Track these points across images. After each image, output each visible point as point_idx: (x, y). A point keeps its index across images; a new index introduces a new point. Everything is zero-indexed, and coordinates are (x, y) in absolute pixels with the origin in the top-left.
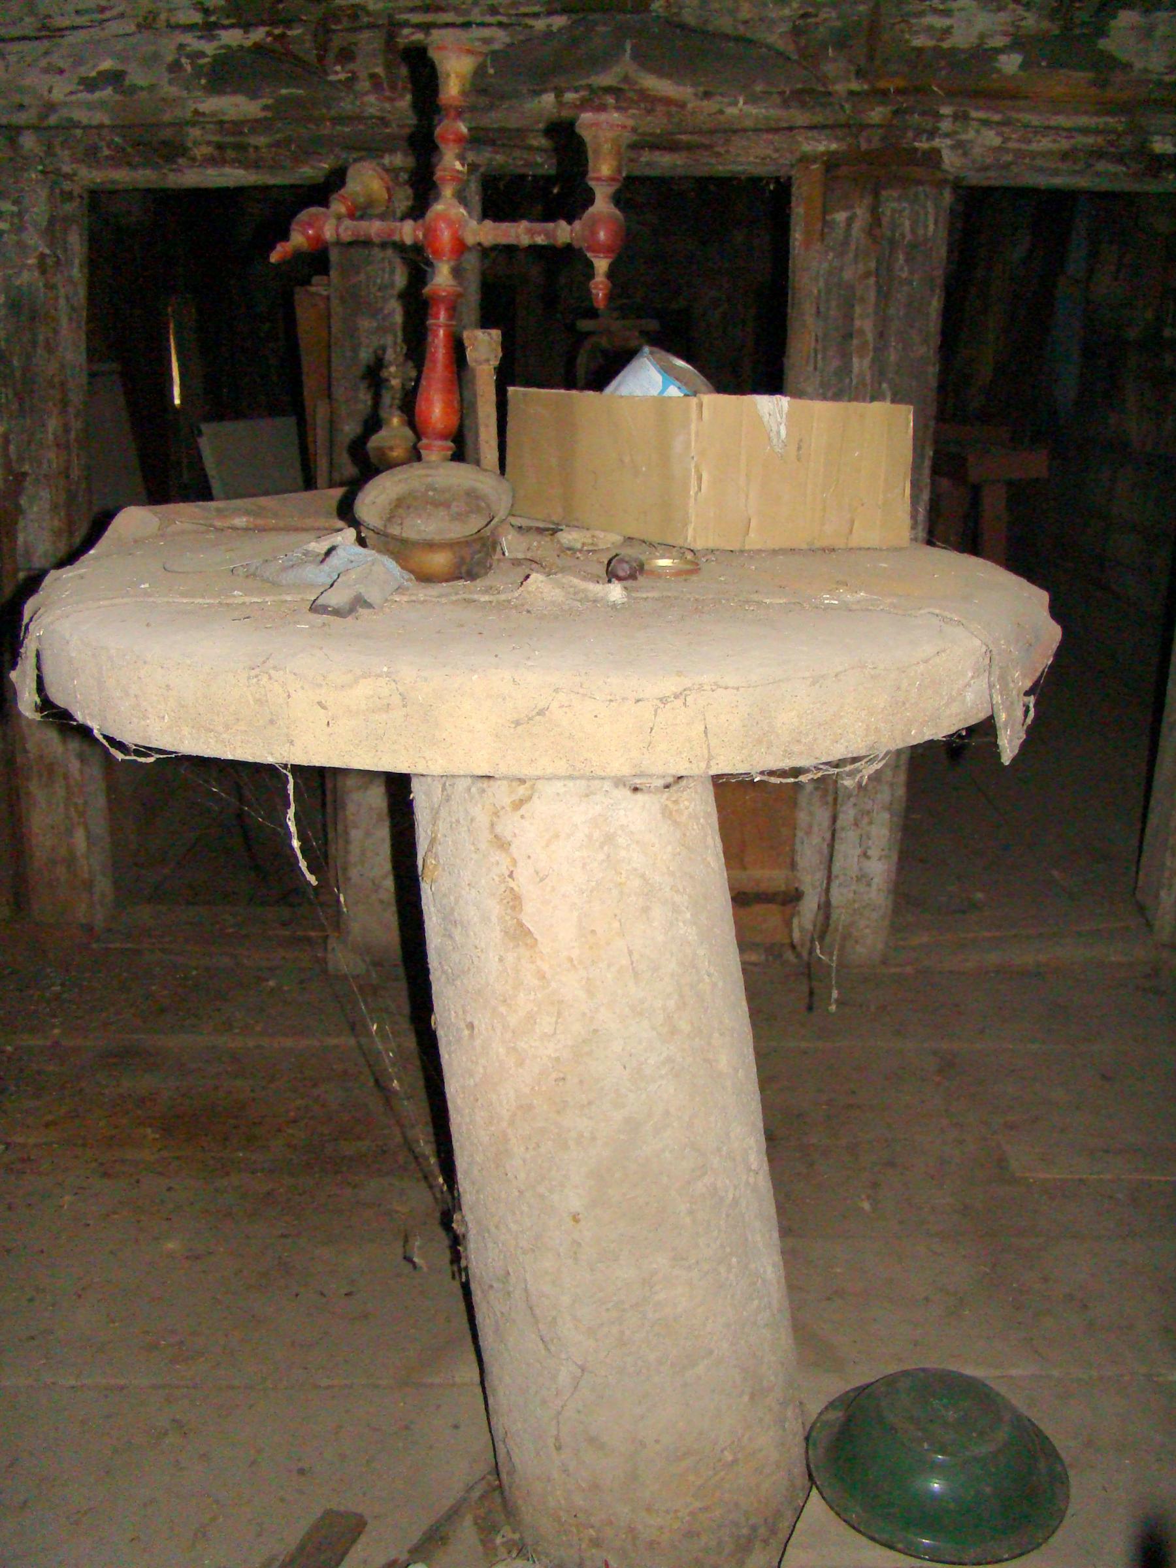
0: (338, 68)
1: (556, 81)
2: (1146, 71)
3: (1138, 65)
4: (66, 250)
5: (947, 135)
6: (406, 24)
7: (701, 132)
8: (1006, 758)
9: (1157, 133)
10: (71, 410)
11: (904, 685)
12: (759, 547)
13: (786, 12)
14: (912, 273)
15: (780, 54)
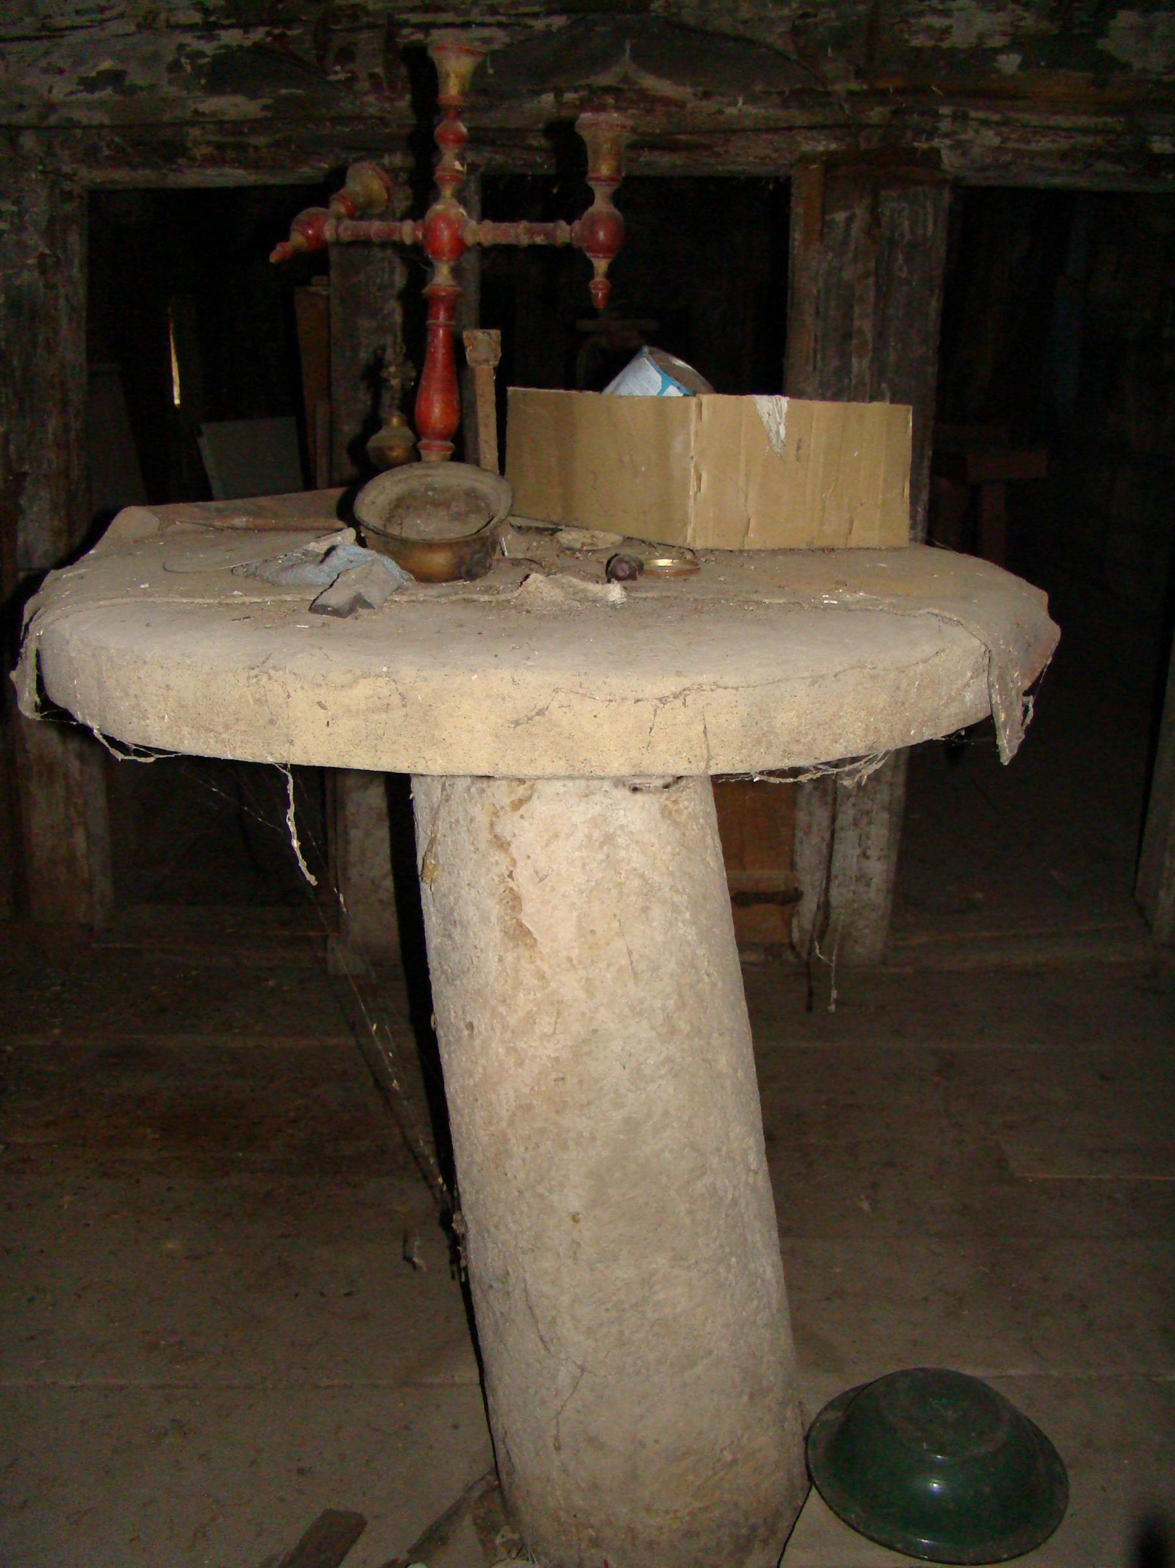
0: (338, 68)
4: (65, 250)
6: (406, 24)
8: (1006, 758)
12: (758, 547)
13: (786, 12)
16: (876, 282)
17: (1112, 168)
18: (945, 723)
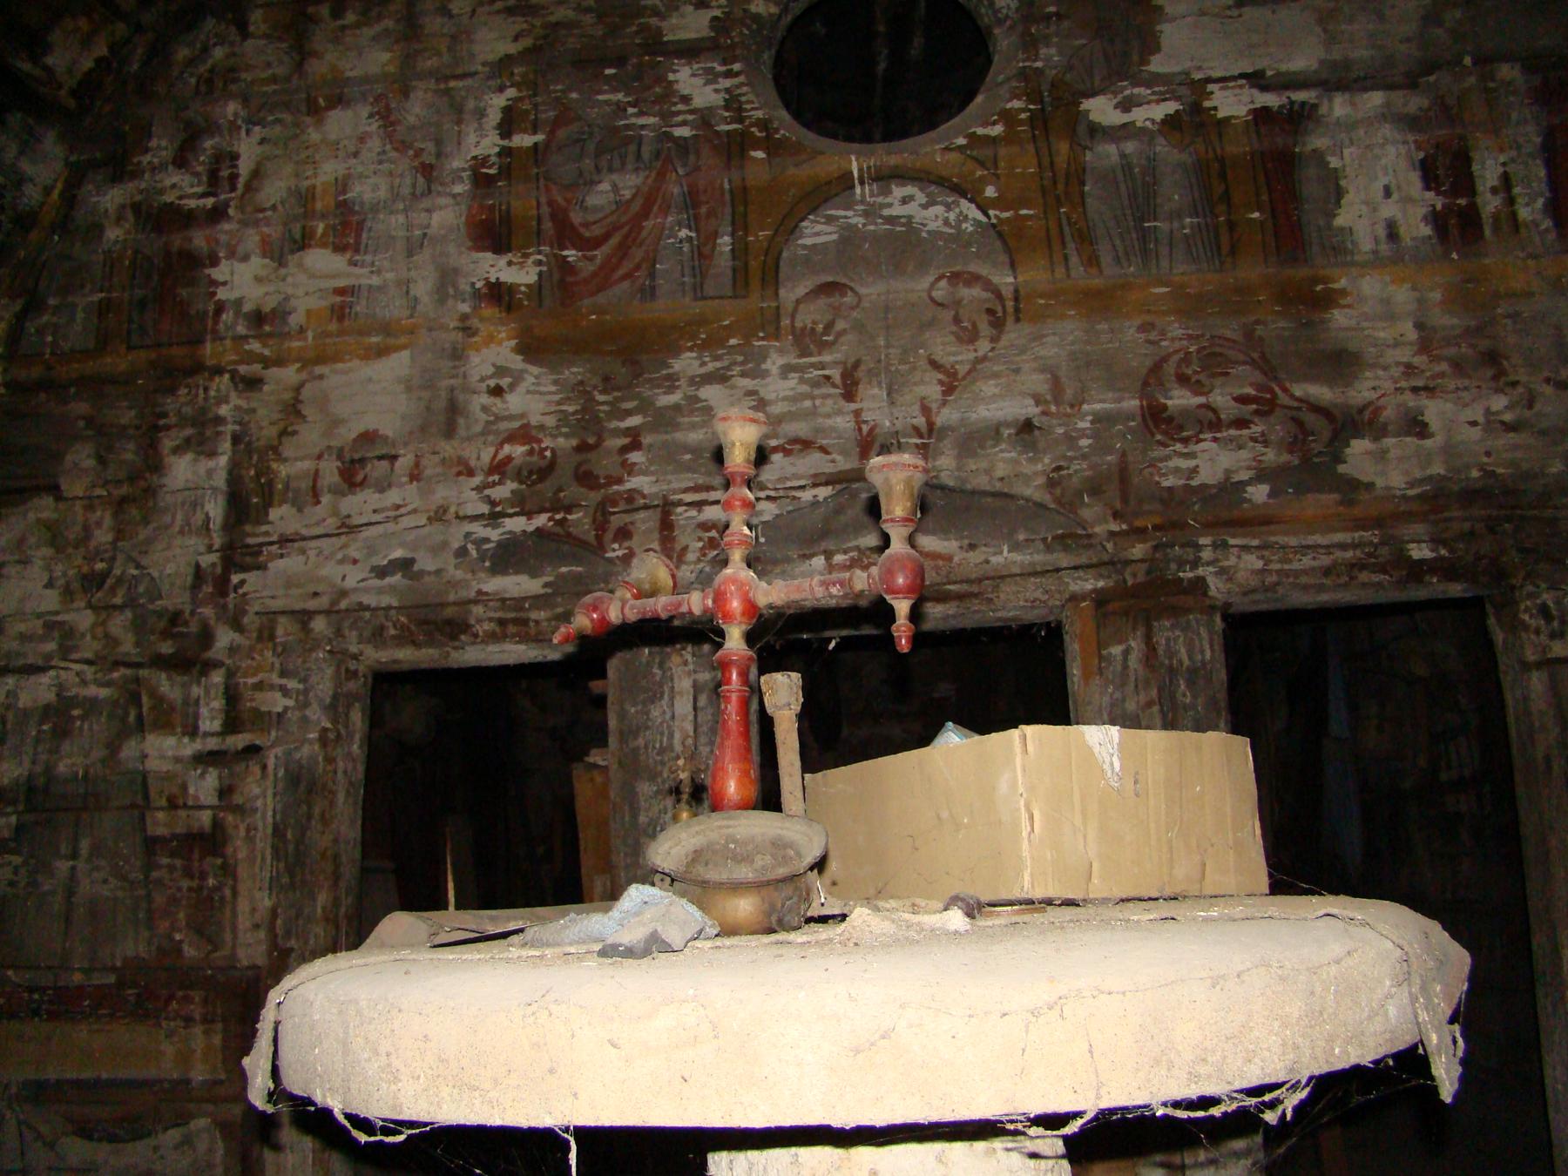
0: (616, 546)
1: (824, 545)
2: (1388, 488)
3: (1380, 483)
4: (347, 727)
5: (1208, 564)
6: (680, 503)
7: (969, 581)
8: (1447, 1092)
9: (1413, 541)
10: (342, 884)
11: (1318, 989)
12: (1105, 895)
13: (1040, 467)
14: (1194, 697)
15: (1037, 504)
16: (1162, 711)
17: (1376, 578)
18: (1372, 1044)
